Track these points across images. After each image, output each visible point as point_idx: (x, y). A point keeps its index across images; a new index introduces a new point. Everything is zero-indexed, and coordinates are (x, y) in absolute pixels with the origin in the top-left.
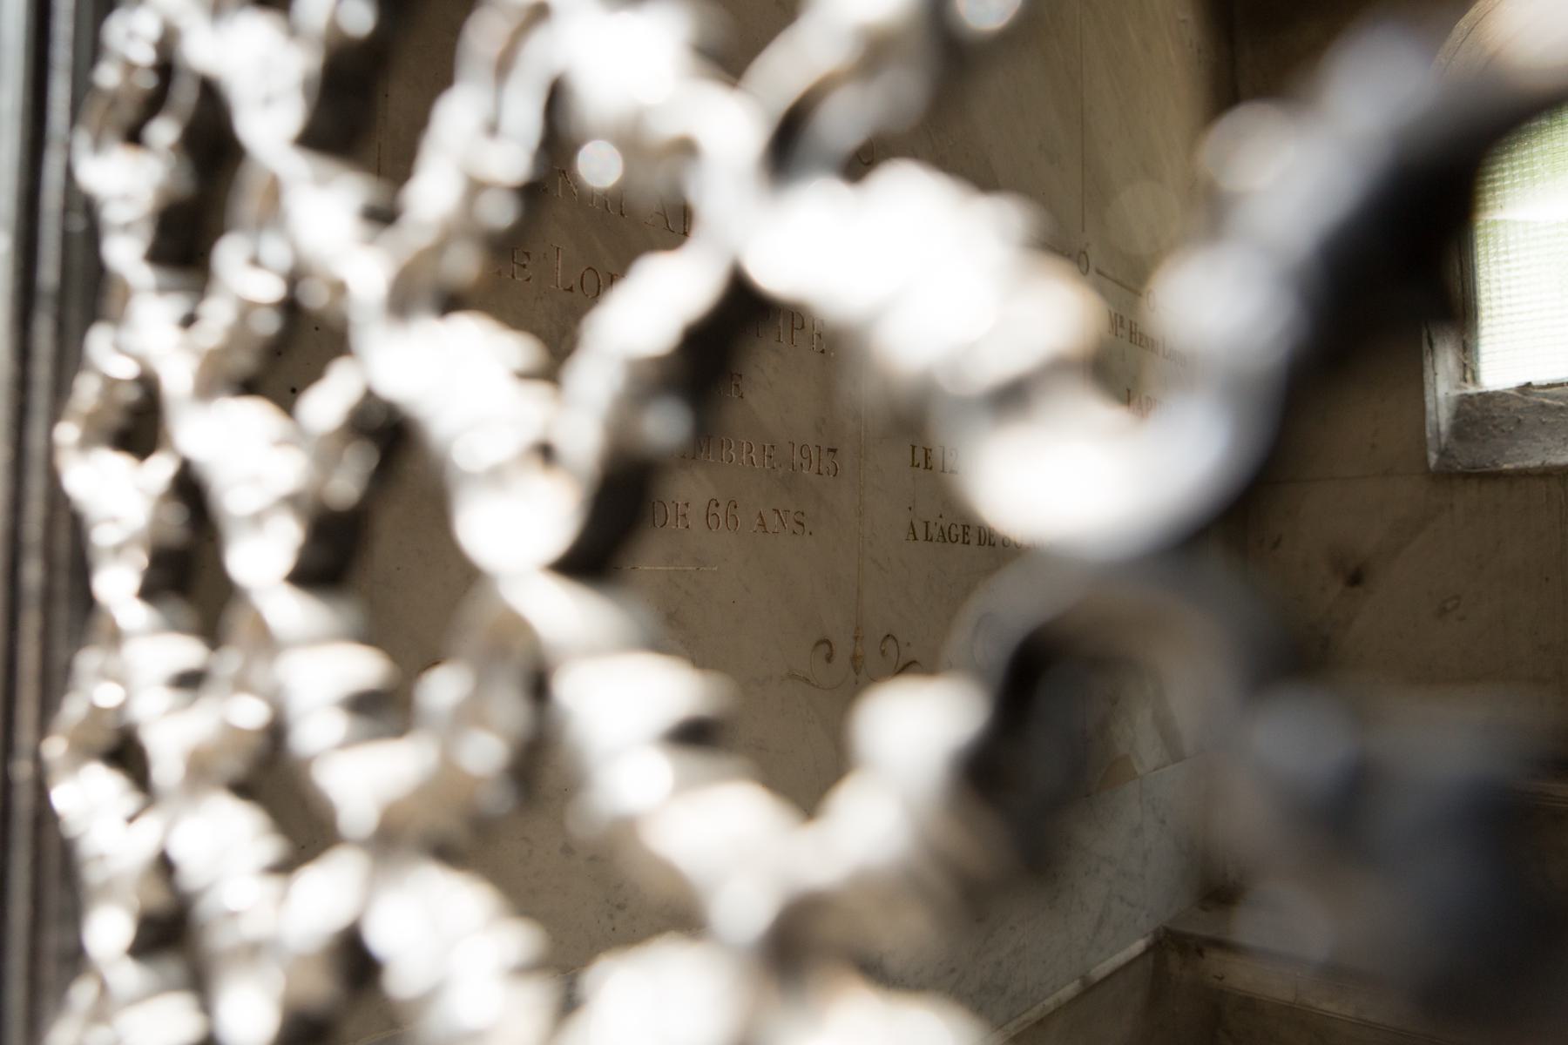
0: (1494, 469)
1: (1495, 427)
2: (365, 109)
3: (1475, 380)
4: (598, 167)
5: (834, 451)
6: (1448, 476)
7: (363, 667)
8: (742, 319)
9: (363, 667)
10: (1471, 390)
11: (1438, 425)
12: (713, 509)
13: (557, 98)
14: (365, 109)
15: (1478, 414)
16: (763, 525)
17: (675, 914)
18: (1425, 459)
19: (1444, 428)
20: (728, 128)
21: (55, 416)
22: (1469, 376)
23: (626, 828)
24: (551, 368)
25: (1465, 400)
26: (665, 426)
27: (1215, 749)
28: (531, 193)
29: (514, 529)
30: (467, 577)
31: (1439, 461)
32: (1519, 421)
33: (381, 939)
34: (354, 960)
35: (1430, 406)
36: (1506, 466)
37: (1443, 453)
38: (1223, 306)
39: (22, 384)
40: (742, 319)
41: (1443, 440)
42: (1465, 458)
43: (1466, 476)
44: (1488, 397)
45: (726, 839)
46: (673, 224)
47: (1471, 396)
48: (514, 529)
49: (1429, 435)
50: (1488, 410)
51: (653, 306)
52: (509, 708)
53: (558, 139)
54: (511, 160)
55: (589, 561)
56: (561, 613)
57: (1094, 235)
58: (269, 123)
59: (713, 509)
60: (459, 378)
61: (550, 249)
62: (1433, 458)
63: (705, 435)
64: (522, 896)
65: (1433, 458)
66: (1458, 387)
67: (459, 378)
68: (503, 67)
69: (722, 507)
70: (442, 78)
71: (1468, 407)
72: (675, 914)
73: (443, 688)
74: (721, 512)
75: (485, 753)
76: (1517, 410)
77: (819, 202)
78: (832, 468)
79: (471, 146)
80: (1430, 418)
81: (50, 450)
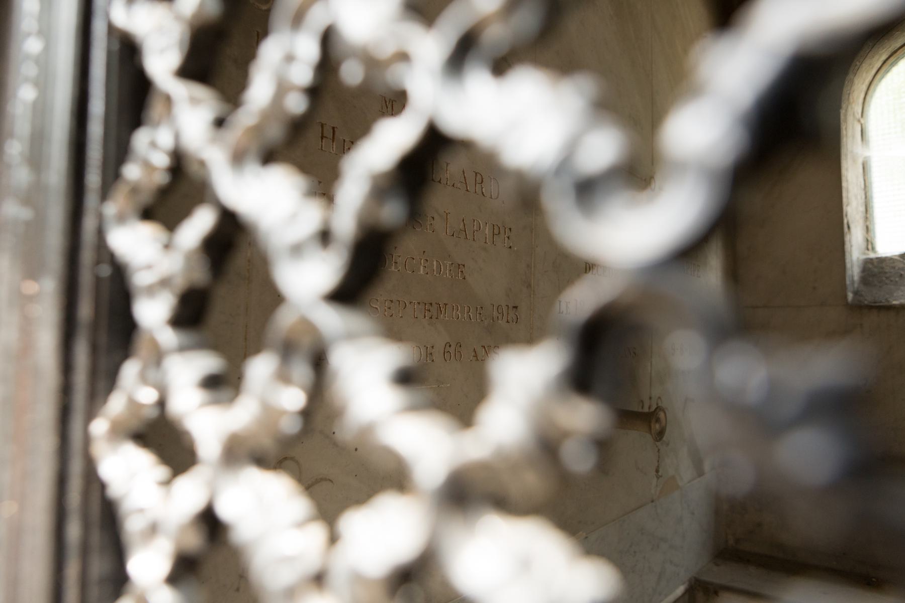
0: (886, 304)
1: (887, 278)
2: (217, 56)
3: (873, 249)
4: (352, 73)
5: (516, 307)
6: (860, 308)
7: (206, 363)
8: (435, 143)
9: (206, 363)
10: (872, 255)
11: (853, 276)
12: (448, 348)
13: (328, 37)
14: (217, 56)
15: (876, 270)
16: (476, 356)
17: (393, 477)
18: (846, 296)
19: (856, 278)
20: (430, 47)
21: (90, 415)
22: (870, 247)
23: (367, 431)
24: (323, 184)
25: (870, 261)
26: (392, 212)
27: (709, 377)
28: (314, 92)
29: (307, 280)
30: (274, 298)
31: (854, 298)
32: (901, 275)
33: (225, 511)
34: (210, 522)
35: (848, 265)
36: (895, 302)
37: (856, 293)
38: (703, 129)
39: (66, 390)
40: (435, 143)
41: (856, 285)
42: (868, 298)
43: (870, 307)
44: (882, 260)
45: (427, 445)
46: (395, 102)
47: (871, 259)
48: (307, 280)
49: (848, 282)
50: (882, 268)
51: (387, 143)
52: (302, 371)
53: (327, 64)
54: (302, 74)
55: (346, 294)
56: (331, 320)
57: (637, 99)
58: (162, 62)
59: (448, 348)
60: (271, 199)
61: (312, 138)
62: (850, 296)
63: (415, 215)
64: (311, 484)
65: (850, 296)
66: (864, 254)
67: (271, 199)
68: (298, 20)
69: (453, 347)
70: (261, 32)
71: (870, 266)
72: (393, 477)
73: (260, 368)
74: (452, 350)
75: (293, 399)
76: (899, 269)
77: (479, 83)
78: (515, 318)
79: (282, 65)
80: (849, 273)
81: (87, 440)
